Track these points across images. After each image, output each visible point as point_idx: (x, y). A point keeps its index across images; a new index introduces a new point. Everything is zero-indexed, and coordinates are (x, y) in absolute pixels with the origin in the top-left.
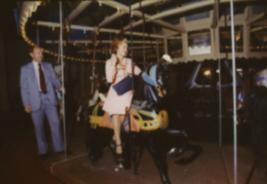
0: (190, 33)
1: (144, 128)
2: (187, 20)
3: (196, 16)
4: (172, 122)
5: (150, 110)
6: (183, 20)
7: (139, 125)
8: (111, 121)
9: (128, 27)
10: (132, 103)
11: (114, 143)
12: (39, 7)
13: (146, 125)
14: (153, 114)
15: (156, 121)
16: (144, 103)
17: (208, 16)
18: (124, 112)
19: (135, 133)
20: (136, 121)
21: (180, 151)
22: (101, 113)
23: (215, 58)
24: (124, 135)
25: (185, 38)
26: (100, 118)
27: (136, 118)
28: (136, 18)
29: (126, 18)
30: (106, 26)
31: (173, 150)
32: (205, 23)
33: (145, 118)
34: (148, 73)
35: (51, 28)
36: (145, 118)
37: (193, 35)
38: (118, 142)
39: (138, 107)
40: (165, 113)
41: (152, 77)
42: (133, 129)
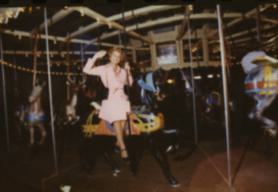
0: (158, 44)
1: (144, 130)
2: (155, 33)
3: (164, 29)
4: (167, 124)
5: (148, 113)
6: (151, 33)
7: (138, 128)
8: (113, 130)
9: (73, 34)
10: (132, 109)
11: (119, 148)
12: (21, 13)
13: (146, 127)
14: (152, 116)
15: (154, 122)
16: (143, 108)
17: (173, 30)
18: (125, 118)
19: (135, 136)
20: (135, 126)
21: (177, 147)
22: (97, 120)
23: (181, 67)
24: (128, 139)
25: (153, 49)
26: (96, 126)
27: (136, 122)
28: (114, 29)
29: (104, 28)
30: (78, 37)
31: (170, 148)
32: (173, 34)
33: (145, 121)
34: (144, 80)
35: (17, 36)
36: (145, 121)
37: (161, 47)
38: (123, 146)
39: (137, 112)
40: (161, 115)
41: (149, 83)
42: (133, 133)
